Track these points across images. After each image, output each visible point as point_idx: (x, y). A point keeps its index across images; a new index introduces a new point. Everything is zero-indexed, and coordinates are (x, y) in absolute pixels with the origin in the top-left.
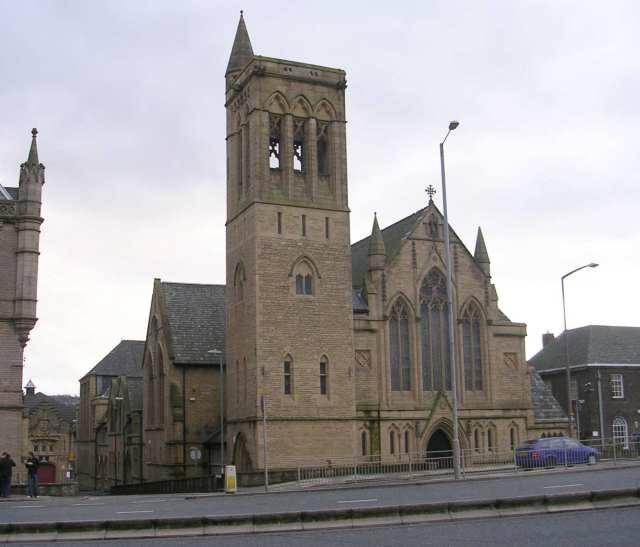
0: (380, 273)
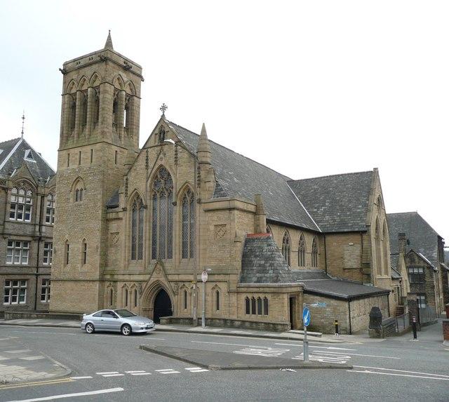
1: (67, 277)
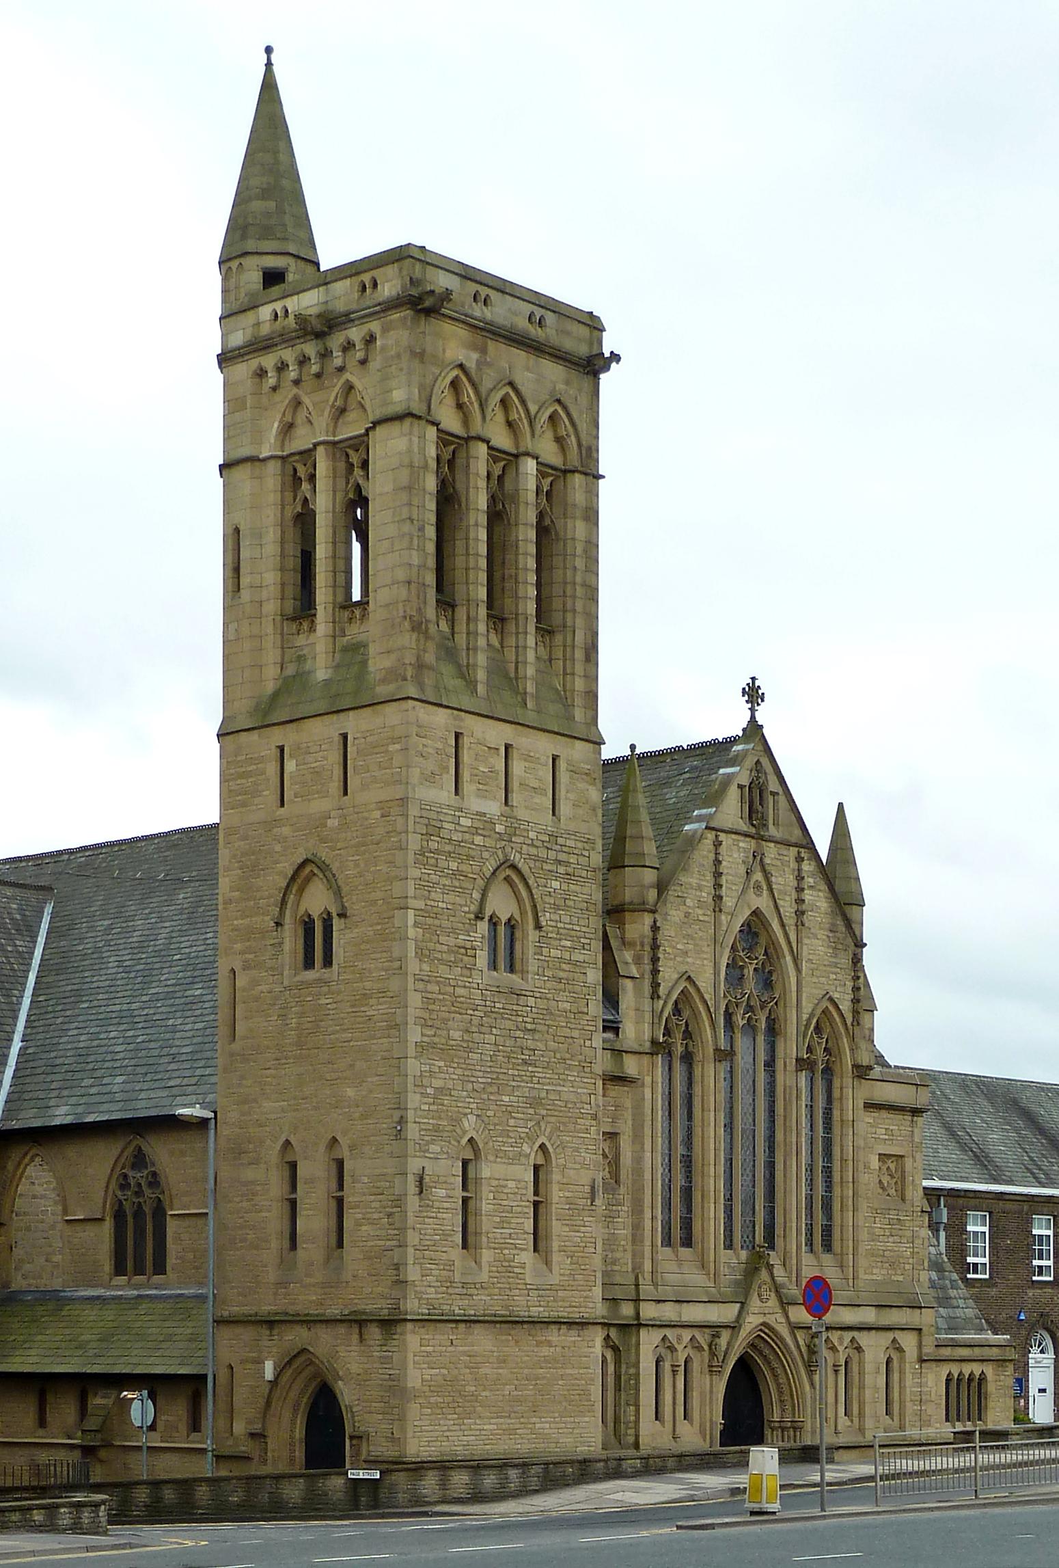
0: (648, 919)
1: (482, 1303)
